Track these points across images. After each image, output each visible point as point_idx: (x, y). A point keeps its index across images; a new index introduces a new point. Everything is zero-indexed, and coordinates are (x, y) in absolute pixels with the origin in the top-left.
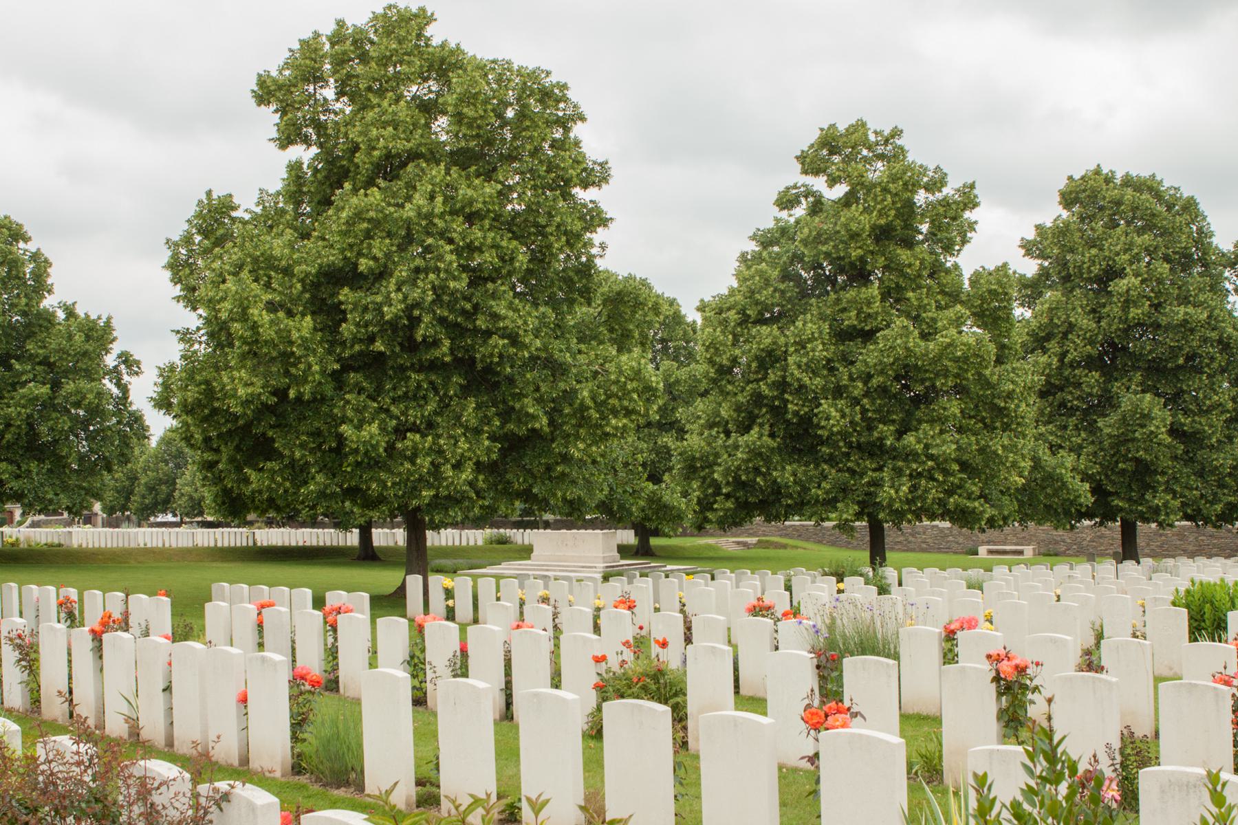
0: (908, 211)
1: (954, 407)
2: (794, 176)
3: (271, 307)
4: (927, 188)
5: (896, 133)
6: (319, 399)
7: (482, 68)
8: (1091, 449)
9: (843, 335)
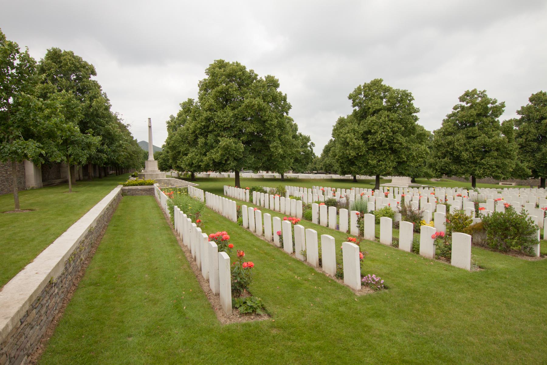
0: (486, 109)
1: (496, 154)
2: (458, 102)
3: (356, 139)
4: (492, 104)
5: (484, 91)
6: (364, 155)
7: (394, 91)
8: (533, 161)
9: (468, 138)
